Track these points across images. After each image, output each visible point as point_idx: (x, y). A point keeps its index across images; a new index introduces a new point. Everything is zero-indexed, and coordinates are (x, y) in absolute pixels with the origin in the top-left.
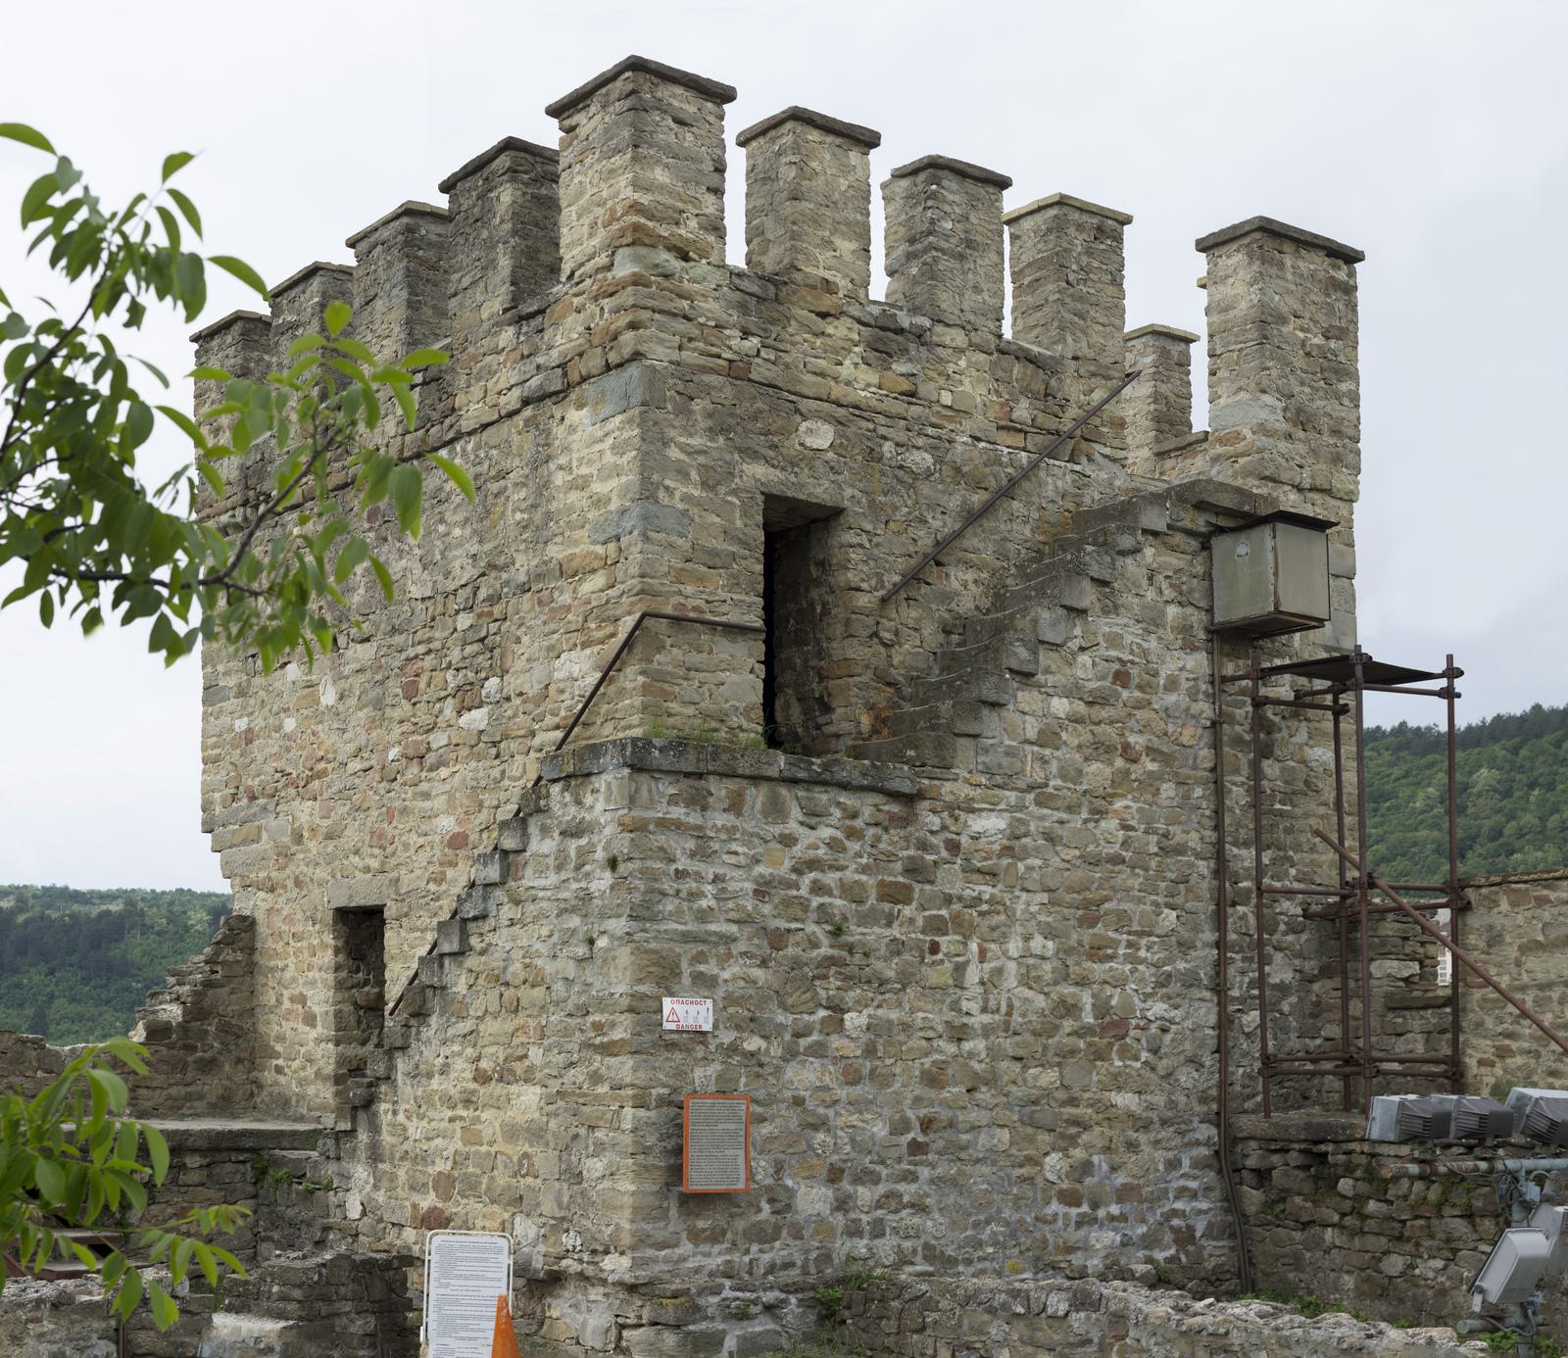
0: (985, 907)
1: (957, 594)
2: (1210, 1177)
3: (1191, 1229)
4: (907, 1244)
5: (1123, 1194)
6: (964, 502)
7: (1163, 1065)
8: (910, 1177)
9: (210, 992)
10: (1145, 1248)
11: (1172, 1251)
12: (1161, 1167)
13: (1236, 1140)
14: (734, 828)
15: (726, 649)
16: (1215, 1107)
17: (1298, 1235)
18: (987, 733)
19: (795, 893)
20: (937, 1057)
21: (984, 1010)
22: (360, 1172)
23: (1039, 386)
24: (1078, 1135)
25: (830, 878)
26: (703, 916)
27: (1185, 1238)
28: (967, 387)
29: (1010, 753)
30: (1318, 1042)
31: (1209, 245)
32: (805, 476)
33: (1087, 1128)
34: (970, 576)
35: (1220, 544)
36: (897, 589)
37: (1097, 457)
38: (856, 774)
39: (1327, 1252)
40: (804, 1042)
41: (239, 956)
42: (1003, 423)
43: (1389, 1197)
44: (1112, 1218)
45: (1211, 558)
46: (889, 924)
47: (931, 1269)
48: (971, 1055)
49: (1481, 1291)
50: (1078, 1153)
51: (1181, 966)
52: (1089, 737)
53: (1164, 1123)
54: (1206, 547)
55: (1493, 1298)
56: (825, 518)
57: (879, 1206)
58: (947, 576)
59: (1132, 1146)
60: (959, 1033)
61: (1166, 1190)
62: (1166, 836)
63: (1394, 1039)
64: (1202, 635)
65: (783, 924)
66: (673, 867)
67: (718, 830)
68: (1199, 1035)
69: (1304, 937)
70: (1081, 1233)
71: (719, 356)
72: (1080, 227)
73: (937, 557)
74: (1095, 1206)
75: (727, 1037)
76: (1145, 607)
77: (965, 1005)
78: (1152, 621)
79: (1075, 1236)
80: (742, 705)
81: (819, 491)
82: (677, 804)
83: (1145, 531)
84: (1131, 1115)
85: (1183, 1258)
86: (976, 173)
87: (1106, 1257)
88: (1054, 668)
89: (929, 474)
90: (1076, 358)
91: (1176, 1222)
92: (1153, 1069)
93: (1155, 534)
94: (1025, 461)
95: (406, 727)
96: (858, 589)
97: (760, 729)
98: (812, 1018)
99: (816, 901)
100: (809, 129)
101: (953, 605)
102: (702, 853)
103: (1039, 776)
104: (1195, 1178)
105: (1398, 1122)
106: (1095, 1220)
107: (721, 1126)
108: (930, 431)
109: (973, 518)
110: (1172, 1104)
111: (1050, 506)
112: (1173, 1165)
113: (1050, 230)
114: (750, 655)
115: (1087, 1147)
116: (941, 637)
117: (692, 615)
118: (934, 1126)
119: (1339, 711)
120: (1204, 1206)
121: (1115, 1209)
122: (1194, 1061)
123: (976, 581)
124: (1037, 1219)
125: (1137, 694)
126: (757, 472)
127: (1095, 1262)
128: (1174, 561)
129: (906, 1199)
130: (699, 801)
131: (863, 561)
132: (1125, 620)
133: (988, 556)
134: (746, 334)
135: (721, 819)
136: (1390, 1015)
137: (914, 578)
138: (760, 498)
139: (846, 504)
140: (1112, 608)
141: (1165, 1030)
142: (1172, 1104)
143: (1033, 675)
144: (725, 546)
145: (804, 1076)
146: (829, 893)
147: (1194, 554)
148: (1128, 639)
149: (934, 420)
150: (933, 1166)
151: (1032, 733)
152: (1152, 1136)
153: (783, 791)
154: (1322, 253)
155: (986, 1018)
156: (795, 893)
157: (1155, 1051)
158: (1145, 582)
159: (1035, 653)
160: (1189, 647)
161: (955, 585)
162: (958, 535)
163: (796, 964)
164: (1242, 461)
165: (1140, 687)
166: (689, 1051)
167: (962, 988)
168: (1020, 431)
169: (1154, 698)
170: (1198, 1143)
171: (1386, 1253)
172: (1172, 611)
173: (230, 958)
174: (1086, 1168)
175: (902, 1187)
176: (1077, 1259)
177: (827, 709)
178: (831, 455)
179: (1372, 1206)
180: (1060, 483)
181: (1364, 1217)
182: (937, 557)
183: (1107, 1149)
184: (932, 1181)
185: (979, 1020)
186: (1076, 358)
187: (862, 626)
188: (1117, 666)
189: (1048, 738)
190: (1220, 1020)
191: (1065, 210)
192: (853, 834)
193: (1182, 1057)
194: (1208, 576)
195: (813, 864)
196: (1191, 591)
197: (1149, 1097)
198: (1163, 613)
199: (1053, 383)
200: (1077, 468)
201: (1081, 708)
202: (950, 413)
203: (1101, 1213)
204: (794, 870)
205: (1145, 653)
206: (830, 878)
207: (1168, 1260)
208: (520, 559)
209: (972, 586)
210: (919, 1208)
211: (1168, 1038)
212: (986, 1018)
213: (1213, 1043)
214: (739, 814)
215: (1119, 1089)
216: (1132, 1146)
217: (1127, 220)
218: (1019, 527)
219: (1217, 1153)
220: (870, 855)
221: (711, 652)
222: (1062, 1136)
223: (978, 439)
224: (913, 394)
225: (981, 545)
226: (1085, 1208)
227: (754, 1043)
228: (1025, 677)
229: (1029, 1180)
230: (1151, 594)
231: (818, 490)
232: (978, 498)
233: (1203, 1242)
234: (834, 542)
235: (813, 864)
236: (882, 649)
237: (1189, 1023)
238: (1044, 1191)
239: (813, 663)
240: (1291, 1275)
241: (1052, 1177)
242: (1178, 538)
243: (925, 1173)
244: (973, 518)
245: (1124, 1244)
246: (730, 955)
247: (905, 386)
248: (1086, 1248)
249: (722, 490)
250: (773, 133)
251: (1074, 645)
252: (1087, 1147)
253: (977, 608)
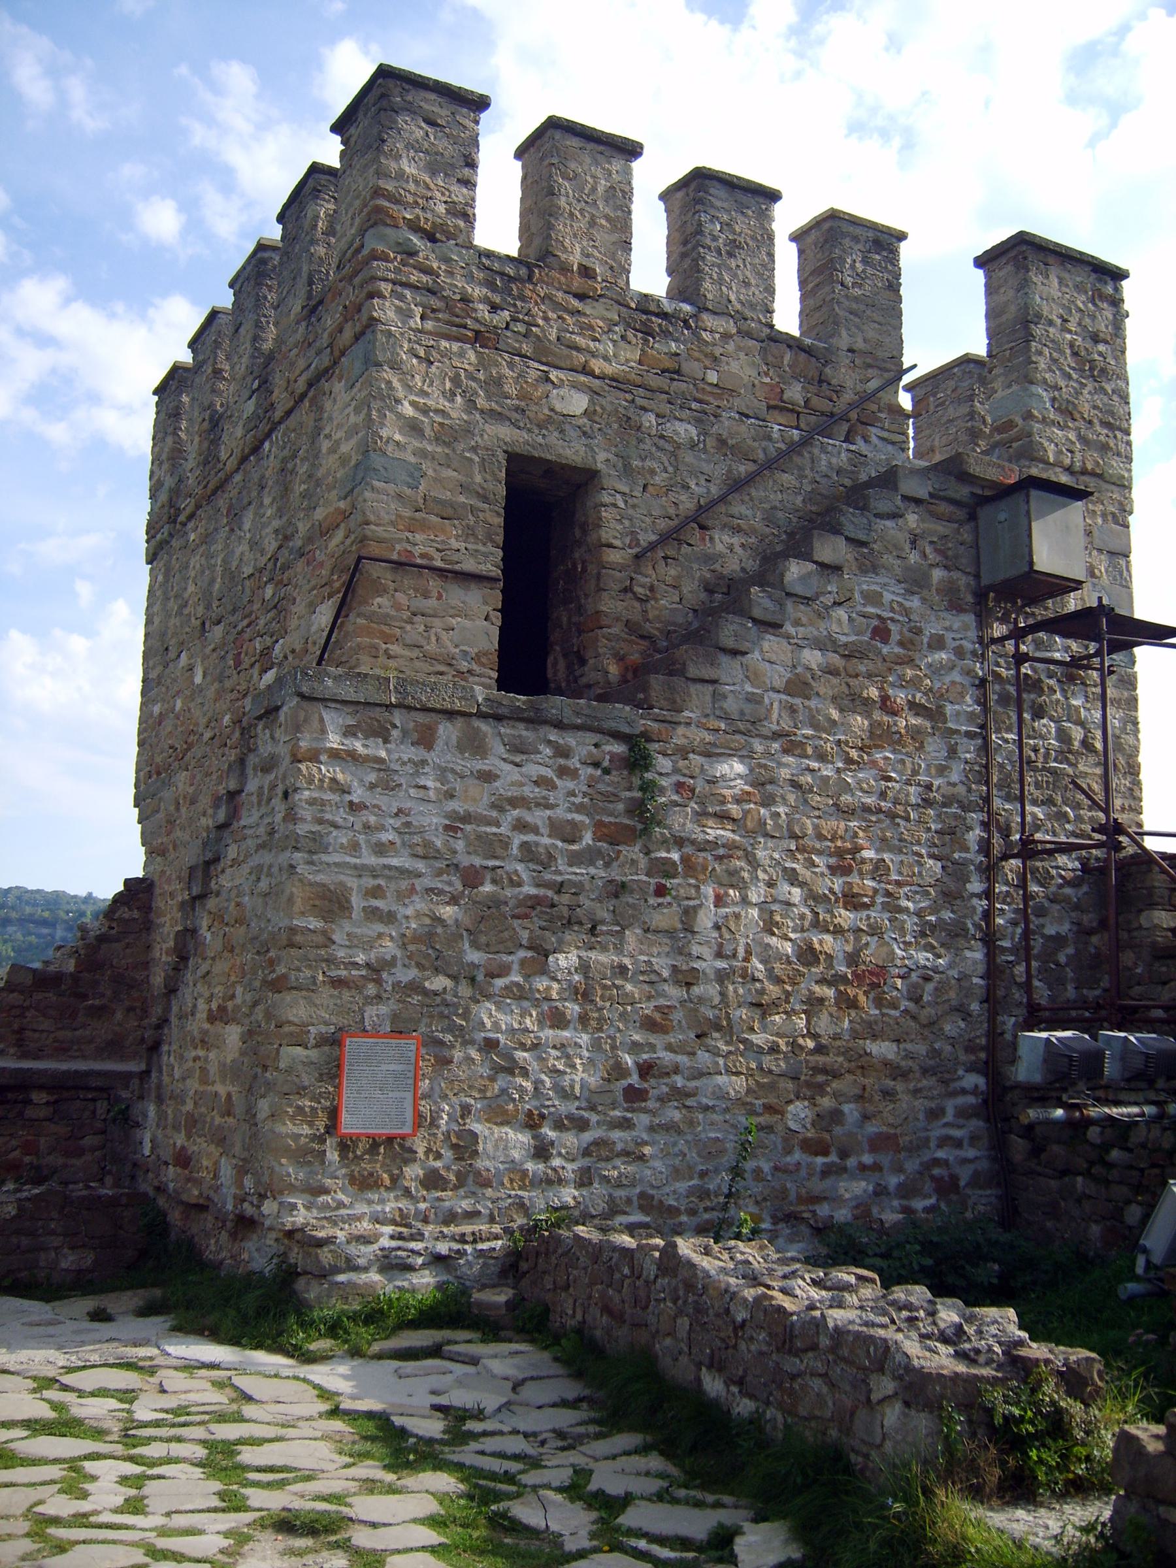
0: (721, 851)
1: (721, 555)
2: (976, 1124)
3: (954, 1178)
4: (620, 1193)
5: (878, 1143)
6: (730, 471)
7: (927, 1013)
8: (625, 1124)
9: (104, 946)
10: (903, 1197)
11: (933, 1201)
12: (921, 1116)
13: (1006, 1089)
14: (424, 762)
15: (457, 595)
16: (983, 1055)
17: (1053, 1183)
18: (724, 679)
19: (494, 830)
20: (662, 1002)
21: (719, 955)
22: (152, 1110)
23: (813, 373)
24: (827, 1083)
25: (538, 817)
26: (381, 849)
27: (947, 1187)
28: (734, 367)
29: (752, 699)
30: (1097, 992)
31: (981, 262)
32: (553, 438)
33: (836, 1075)
34: (736, 540)
35: (984, 513)
36: (652, 547)
37: (874, 439)
38: (568, 712)
39: (1079, 1201)
40: (833, 1158)
41: (136, 914)
42: (772, 403)
43: (1130, 1145)
44: (863, 1168)
45: (976, 528)
46: (607, 865)
47: (648, 1219)
48: (701, 1000)
49: (1145, 1251)
50: (826, 1102)
51: (947, 915)
52: (844, 689)
53: (925, 1071)
54: (972, 517)
55: (1157, 1259)
56: (583, 481)
57: (586, 1153)
58: (711, 539)
59: (888, 1094)
60: (687, 978)
61: (927, 1139)
62: (929, 787)
63: (1160, 988)
64: (970, 599)
65: (478, 861)
66: (348, 798)
67: (404, 764)
68: (964, 984)
69: (1085, 888)
70: (828, 1182)
71: (465, 327)
72: (856, 239)
73: (700, 518)
74: (844, 1154)
75: (407, 975)
76: (908, 569)
77: (696, 950)
78: (915, 582)
79: (817, 1186)
80: (473, 651)
81: (568, 452)
82: (354, 735)
83: (905, 498)
84: (886, 1063)
85: (943, 1206)
86: (742, 184)
87: (857, 1207)
88: (804, 620)
89: (693, 446)
90: (850, 350)
91: (936, 1171)
92: (914, 1018)
93: (918, 501)
94: (796, 438)
95: (235, 695)
96: (610, 546)
97: (495, 675)
98: (510, 958)
99: (518, 839)
100: (567, 135)
101: (717, 566)
102: (387, 785)
103: (786, 724)
104: (960, 1127)
105: (1045, 1061)
106: (844, 1169)
107: (384, 1067)
108: (694, 405)
109: (737, 486)
110: (935, 1053)
111: (823, 481)
112: (935, 1114)
113: (826, 241)
114: (486, 603)
115: (836, 1095)
116: (703, 596)
117: (419, 561)
118: (655, 1071)
119: (1106, 673)
120: (971, 1153)
121: (867, 1159)
122: (961, 1010)
123: (742, 545)
124: (776, 1168)
125: (897, 650)
126: (505, 432)
127: (843, 1211)
128: (941, 528)
129: (619, 1146)
130: (382, 733)
131: (621, 519)
132: (887, 580)
133: (757, 522)
134: (494, 308)
135: (410, 753)
136: (1157, 964)
137: (672, 537)
138: (502, 457)
139: (600, 466)
140: (869, 566)
141: (927, 979)
142: (935, 1053)
143: (781, 626)
144: (462, 499)
145: (495, 1018)
146: (535, 830)
147: (961, 523)
148: (887, 597)
149: (699, 396)
150: (653, 1113)
151: (779, 683)
152: (911, 1086)
153: (484, 727)
154: (1088, 269)
155: (721, 964)
156: (494, 830)
157: (917, 1000)
158: (907, 547)
159: (782, 605)
160: (956, 607)
161: (720, 547)
162: (722, 499)
163: (495, 903)
164: (1014, 445)
165: (901, 644)
166: (359, 988)
167: (693, 932)
168: (792, 411)
169: (917, 656)
170: (964, 1091)
171: (1128, 1202)
172: (937, 574)
173: (126, 916)
174: (836, 1116)
175: (616, 1135)
176: (823, 1210)
177: (583, 662)
178: (584, 420)
179: (1115, 1154)
180: (834, 460)
181: (1110, 1165)
182: (700, 518)
183: (860, 1098)
184: (652, 1129)
185: (709, 964)
186: (850, 350)
187: (614, 580)
188: (875, 622)
189: (799, 686)
190: (988, 969)
191: (836, 223)
192: (563, 772)
193: (946, 1006)
194: (976, 546)
195: (514, 802)
196: (956, 557)
197: (909, 1046)
198: (927, 576)
199: (828, 370)
200: (853, 447)
201: (836, 660)
202: (716, 391)
203: (851, 1162)
204: (493, 806)
205: (907, 612)
206: (538, 817)
207: (927, 1210)
208: (300, 525)
209: (739, 550)
210: (634, 1155)
211: (930, 987)
212: (721, 964)
213: (980, 993)
214: (429, 747)
215: (874, 1037)
216: (888, 1094)
217: (902, 236)
218: (785, 493)
219: (985, 1101)
220: (585, 795)
221: (440, 597)
222: (808, 1084)
223: (747, 416)
224: (678, 372)
225: (749, 513)
226: (833, 1158)
227: (439, 983)
228: (772, 626)
229: (769, 1129)
230: (913, 558)
231: (570, 451)
232: (743, 469)
233: (969, 1191)
234: (589, 504)
235: (514, 802)
236: (637, 604)
237: (954, 973)
238: (785, 1140)
239: (575, 619)
240: (1049, 1224)
241: (792, 1125)
242: (943, 508)
243: (643, 1120)
244: (737, 486)
245: (876, 1193)
246: (412, 890)
247: (668, 364)
248: (836, 1200)
249: (460, 447)
250: (539, 142)
251: (828, 600)
252: (836, 1095)
253: (743, 570)
